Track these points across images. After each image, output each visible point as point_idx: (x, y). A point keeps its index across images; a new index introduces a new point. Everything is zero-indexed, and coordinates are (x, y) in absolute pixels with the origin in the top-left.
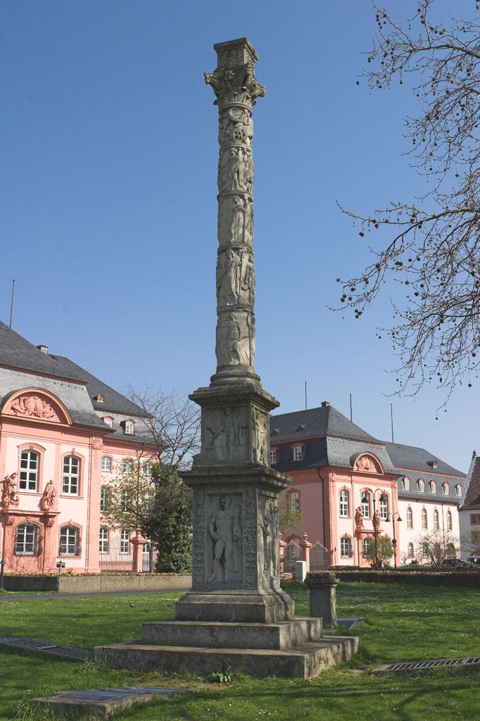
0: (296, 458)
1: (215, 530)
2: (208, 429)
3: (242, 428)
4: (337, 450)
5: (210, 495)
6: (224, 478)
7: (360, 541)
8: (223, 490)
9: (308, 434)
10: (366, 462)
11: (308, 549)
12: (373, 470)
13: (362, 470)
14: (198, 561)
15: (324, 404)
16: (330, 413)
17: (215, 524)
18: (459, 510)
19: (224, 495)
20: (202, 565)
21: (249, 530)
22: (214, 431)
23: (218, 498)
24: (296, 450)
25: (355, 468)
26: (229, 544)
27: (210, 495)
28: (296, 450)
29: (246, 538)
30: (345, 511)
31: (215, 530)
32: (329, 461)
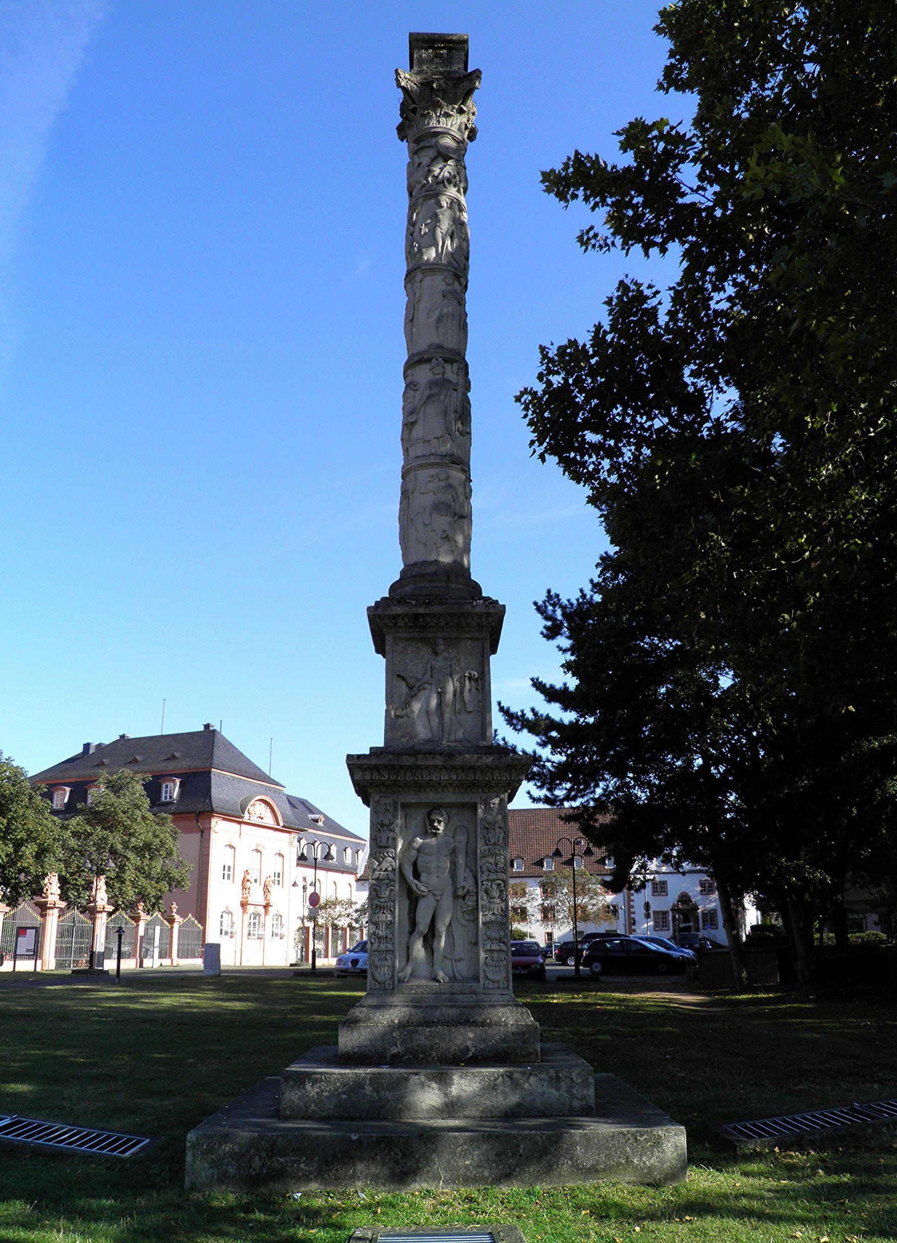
0: (166, 798)
1: (417, 875)
2: (399, 676)
3: (470, 678)
4: (223, 786)
5: (404, 806)
6: (496, 773)
7: (246, 917)
8: (431, 797)
9: (186, 764)
10: (261, 809)
11: (176, 926)
12: (269, 820)
13: (254, 820)
14: (379, 938)
15: (207, 726)
16: (216, 740)
17: (415, 865)
18: (358, 880)
19: (434, 808)
20: (390, 946)
21: (493, 876)
22: (410, 681)
23: (425, 811)
24: (167, 787)
25: (246, 815)
26: (447, 902)
27: (404, 806)
28: (167, 787)
29: (487, 892)
30: (229, 875)
31: (417, 875)
32: (214, 806)
